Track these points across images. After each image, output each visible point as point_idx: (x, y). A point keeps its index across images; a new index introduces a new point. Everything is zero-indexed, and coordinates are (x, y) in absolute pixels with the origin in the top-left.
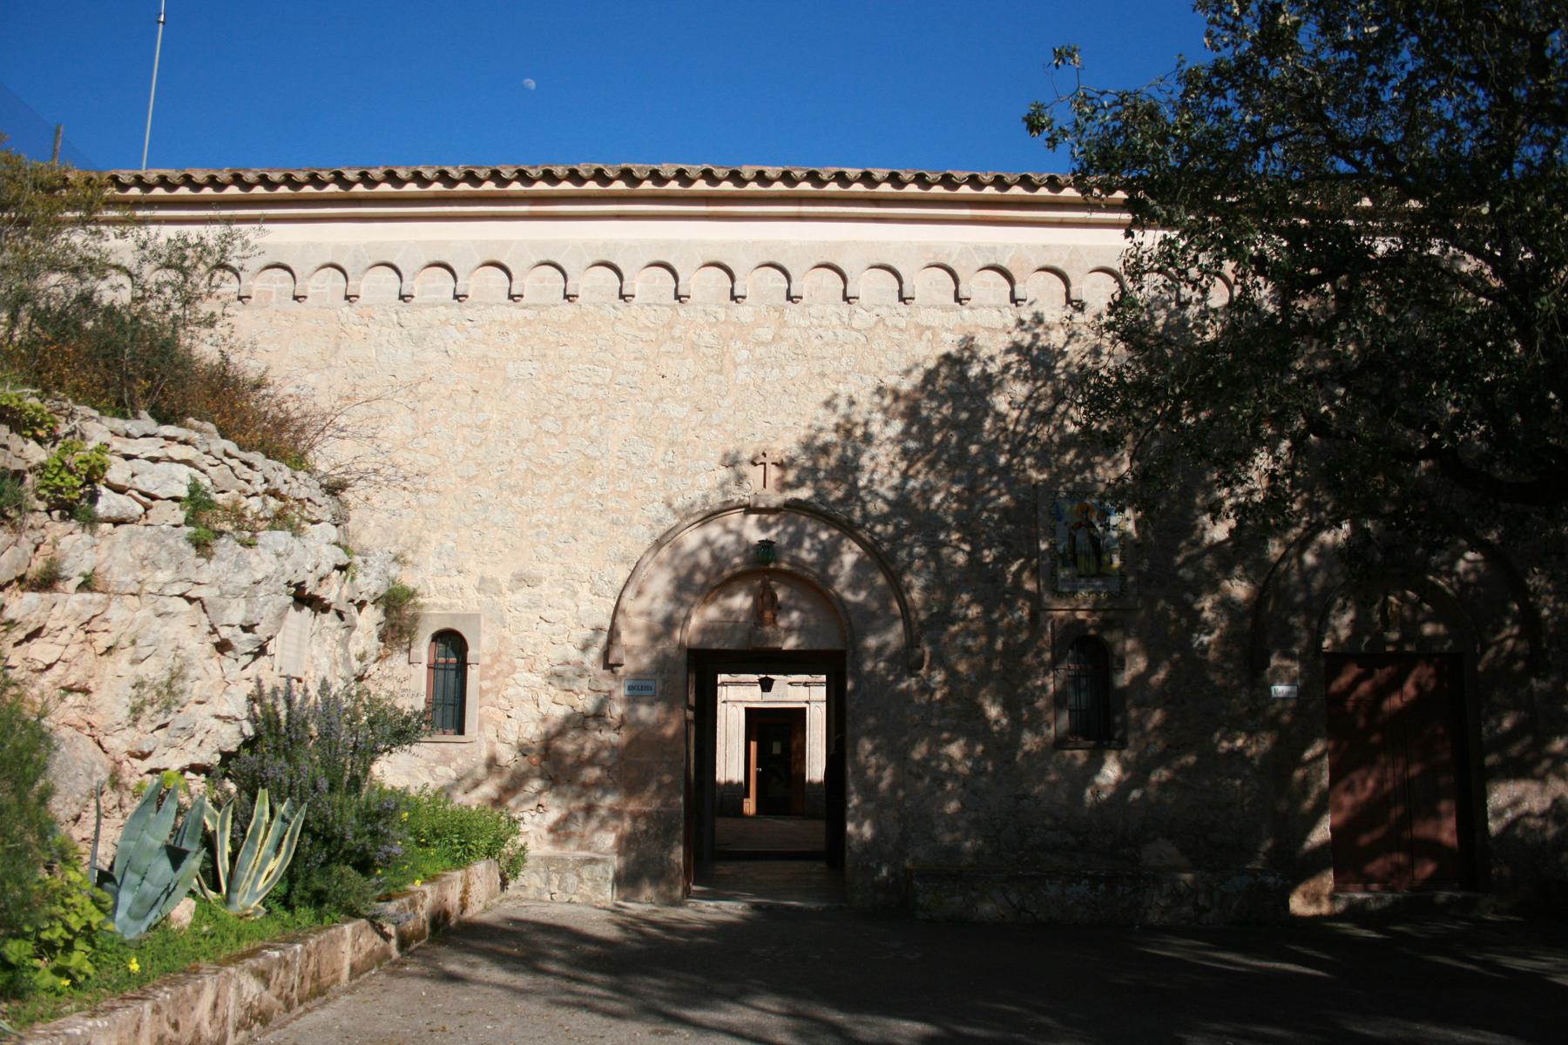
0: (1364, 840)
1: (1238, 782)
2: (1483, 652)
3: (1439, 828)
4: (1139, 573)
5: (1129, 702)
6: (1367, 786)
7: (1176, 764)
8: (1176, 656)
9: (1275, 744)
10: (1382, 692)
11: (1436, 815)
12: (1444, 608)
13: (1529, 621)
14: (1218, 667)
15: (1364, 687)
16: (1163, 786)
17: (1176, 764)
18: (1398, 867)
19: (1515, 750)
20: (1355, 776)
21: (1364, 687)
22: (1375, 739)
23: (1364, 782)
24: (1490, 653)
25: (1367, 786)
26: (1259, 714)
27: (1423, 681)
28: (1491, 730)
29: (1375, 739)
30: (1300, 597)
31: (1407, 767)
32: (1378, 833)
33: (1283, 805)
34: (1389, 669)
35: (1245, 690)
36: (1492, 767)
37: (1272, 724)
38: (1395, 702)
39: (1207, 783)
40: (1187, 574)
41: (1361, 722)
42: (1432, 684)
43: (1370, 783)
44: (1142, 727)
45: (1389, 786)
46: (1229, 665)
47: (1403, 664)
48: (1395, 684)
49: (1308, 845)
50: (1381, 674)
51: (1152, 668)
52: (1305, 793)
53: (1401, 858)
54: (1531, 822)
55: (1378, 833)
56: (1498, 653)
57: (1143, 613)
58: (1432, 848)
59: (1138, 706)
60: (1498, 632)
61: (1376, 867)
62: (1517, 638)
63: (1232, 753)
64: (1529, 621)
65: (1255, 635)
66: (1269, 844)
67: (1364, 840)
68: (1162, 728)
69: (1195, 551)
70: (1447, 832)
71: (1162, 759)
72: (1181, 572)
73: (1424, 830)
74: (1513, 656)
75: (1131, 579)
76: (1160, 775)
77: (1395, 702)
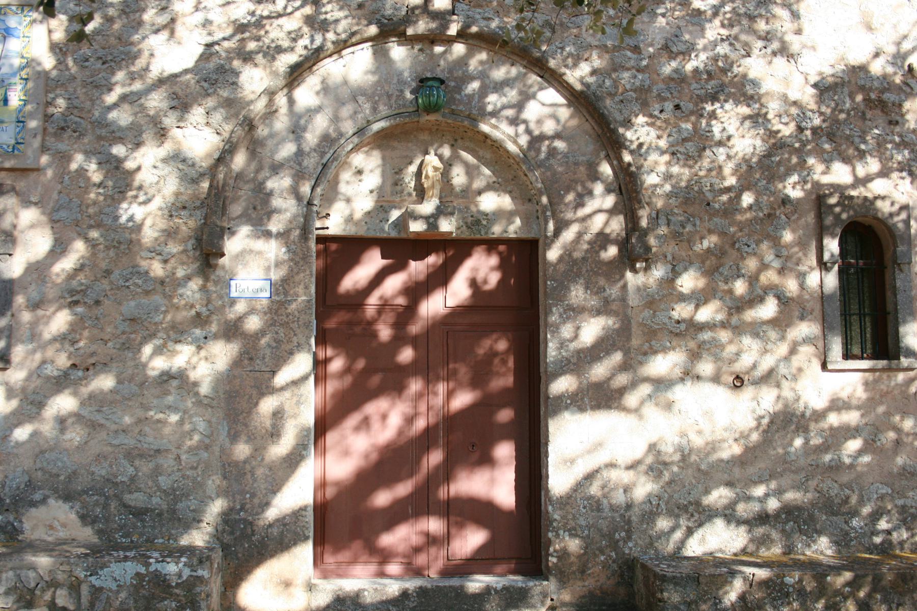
0: (382, 498)
1: (174, 418)
2: (557, 233)
3: (492, 481)
4: (47, 118)
5: (20, 300)
6: (390, 419)
7: (85, 391)
8: (94, 234)
9: (236, 363)
10: (417, 292)
11: (486, 460)
12: (508, 170)
13: (628, 188)
14: (155, 251)
15: (394, 283)
16: (62, 421)
17: (85, 391)
18: (431, 540)
19: (599, 371)
20: (373, 408)
21: (394, 283)
22: (406, 355)
23: (384, 417)
24: (569, 235)
25: (390, 419)
26: (212, 320)
27: (480, 276)
28: (562, 345)
29: (406, 355)
30: (288, 150)
31: (450, 394)
32: (403, 489)
33: (242, 450)
34: (432, 259)
35: (194, 285)
36: (560, 398)
37: (232, 331)
38: (434, 306)
39: (127, 420)
40: (122, 117)
41: (385, 332)
42: (494, 279)
43: (395, 420)
44: (34, 336)
45: (421, 424)
46: (174, 248)
47: (456, 250)
48: (440, 278)
49: (272, 514)
50: (417, 268)
51: (59, 249)
52: (275, 434)
53: (434, 525)
54: (615, 475)
55: (403, 489)
56: (580, 235)
57: (50, 173)
58: (478, 511)
59: (35, 306)
60: (580, 204)
61: (399, 537)
62: (612, 212)
63: (167, 377)
64: (628, 188)
65: (213, 210)
66: (217, 507)
67: (382, 498)
68: (66, 339)
69: (137, 86)
70: (498, 485)
71: (61, 382)
72: (113, 115)
73: (470, 484)
74: (602, 239)
75: (33, 124)
76: (64, 403)
77: (434, 306)
